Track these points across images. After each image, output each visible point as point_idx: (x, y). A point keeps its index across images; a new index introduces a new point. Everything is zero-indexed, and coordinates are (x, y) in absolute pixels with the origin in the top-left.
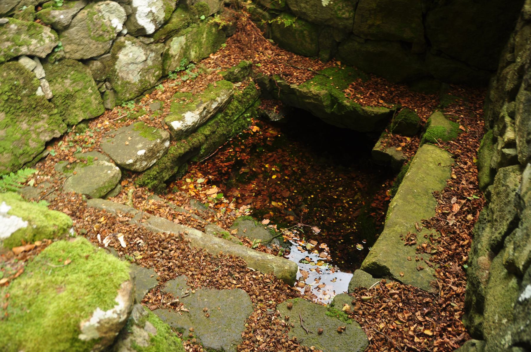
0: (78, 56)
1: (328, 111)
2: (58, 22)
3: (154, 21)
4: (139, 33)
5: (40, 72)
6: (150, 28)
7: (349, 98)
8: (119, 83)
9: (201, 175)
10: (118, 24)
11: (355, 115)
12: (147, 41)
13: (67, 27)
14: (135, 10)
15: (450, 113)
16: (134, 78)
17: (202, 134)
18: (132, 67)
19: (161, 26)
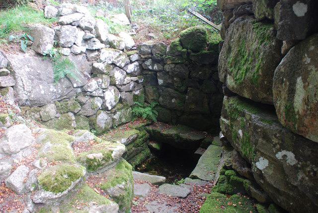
0: (85, 114)
1: (176, 141)
2: (82, 102)
3: (111, 105)
4: (105, 109)
5: (74, 118)
6: (110, 108)
7: (185, 136)
8: (297, 117)
9: (222, 119)
10: (99, 105)
11: (187, 142)
12: (108, 112)
13: (84, 104)
14: (106, 101)
15: (244, 76)
16: (103, 126)
17: (149, 146)
18: (102, 121)
19: (114, 107)
